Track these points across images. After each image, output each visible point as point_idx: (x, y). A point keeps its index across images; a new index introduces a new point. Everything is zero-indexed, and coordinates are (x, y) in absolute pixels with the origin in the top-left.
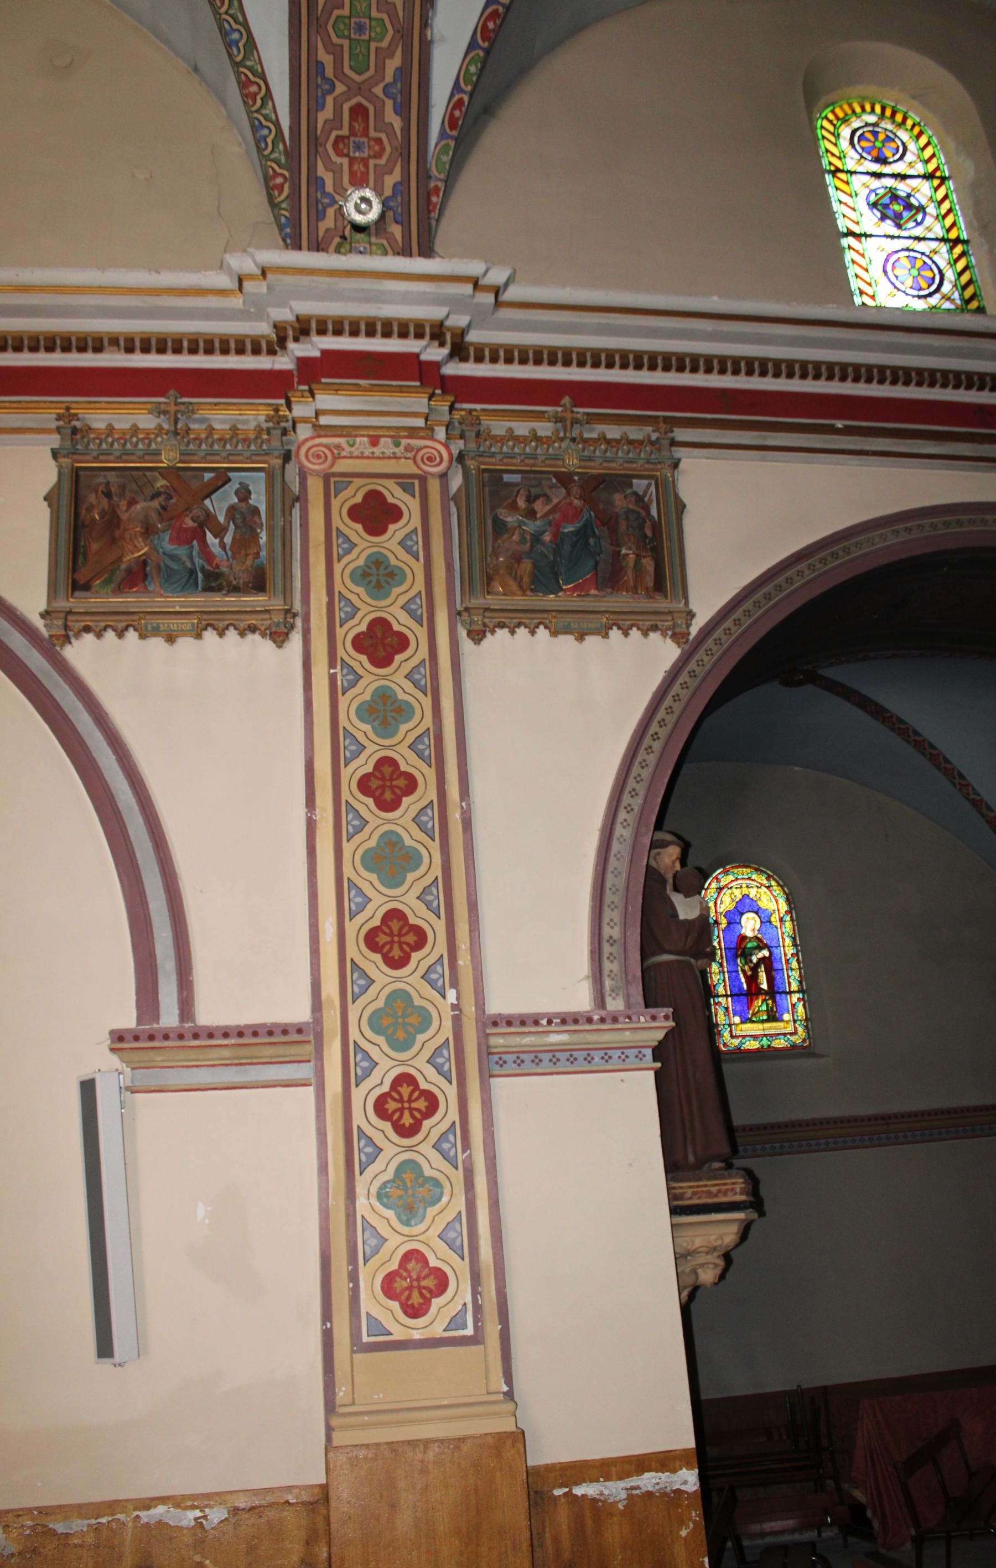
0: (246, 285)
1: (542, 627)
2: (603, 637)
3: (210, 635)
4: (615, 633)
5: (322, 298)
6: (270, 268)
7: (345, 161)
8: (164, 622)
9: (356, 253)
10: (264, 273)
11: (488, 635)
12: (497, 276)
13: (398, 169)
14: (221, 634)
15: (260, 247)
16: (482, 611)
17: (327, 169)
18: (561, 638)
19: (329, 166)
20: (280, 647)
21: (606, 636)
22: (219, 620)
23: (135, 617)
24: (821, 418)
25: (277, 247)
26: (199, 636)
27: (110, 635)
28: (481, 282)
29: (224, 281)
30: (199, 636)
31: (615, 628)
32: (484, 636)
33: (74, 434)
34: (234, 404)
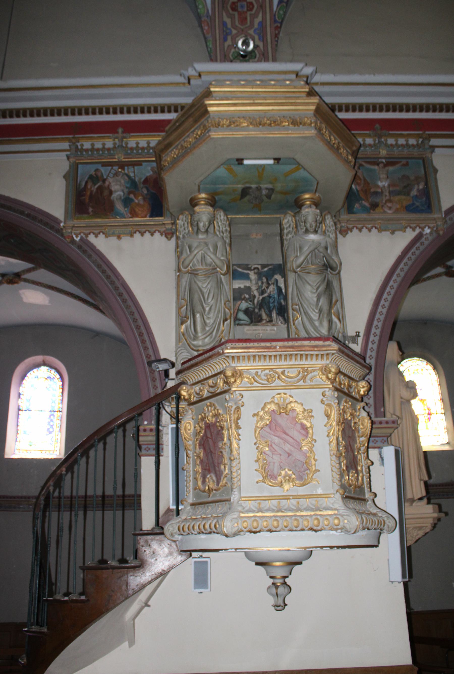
0: (192, 82)
1: (374, 228)
2: (403, 232)
3: (137, 235)
4: (137, 235)
5: (271, 88)
6: (203, 72)
7: (236, 13)
8: (117, 230)
9: (228, 61)
10: (200, 75)
11: (349, 232)
12: (308, 70)
13: (260, 15)
14: (142, 235)
15: (200, 61)
16: (346, 221)
17: (228, 17)
18: (384, 233)
19: (229, 16)
20: (344, 237)
21: (405, 231)
22: (96, 230)
23: (104, 228)
24: (410, 130)
25: (208, 62)
26: (132, 236)
27: (147, 235)
28: (299, 74)
29: (182, 80)
30: (132, 236)
31: (408, 228)
32: (347, 233)
33: (75, 152)
34: (141, 136)
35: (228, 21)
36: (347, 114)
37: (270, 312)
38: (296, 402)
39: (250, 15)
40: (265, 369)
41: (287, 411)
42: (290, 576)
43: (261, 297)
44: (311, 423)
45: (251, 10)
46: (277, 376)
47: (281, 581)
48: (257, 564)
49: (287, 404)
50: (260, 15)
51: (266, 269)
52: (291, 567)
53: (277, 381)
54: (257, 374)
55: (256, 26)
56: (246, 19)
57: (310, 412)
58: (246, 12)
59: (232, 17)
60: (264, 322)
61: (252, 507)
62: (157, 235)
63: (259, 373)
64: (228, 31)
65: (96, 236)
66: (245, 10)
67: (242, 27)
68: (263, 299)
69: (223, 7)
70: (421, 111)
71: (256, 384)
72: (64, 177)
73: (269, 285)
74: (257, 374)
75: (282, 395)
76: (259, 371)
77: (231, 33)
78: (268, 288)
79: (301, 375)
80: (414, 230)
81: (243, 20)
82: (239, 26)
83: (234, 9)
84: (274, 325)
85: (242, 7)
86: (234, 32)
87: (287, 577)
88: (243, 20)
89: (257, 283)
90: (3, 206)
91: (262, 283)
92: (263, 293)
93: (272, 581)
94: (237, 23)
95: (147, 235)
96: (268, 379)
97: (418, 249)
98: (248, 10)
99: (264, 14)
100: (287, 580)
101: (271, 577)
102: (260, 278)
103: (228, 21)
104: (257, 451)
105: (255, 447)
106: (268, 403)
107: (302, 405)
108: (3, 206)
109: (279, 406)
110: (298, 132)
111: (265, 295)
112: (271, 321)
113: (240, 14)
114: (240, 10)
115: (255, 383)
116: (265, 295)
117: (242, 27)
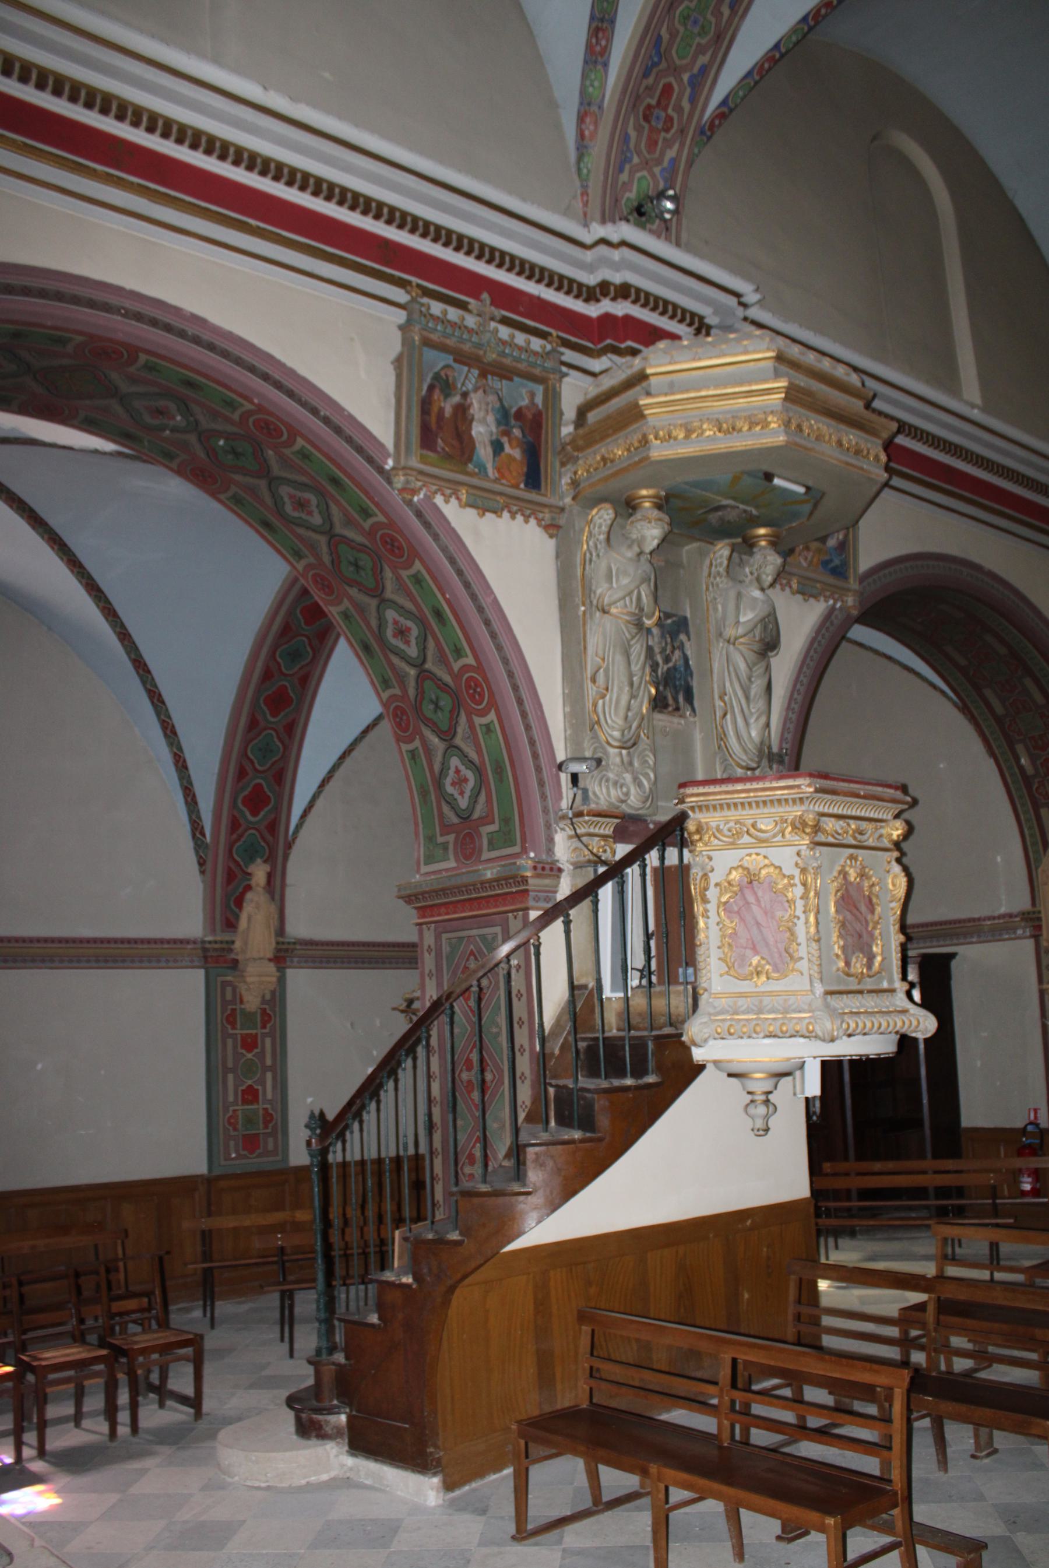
7: (646, 125)
13: (676, 147)
27: (519, 518)
35: (632, 133)
36: (205, 158)
37: (677, 693)
39: (665, 139)
42: (775, 1092)
43: (665, 668)
45: (667, 130)
47: (763, 1097)
48: (730, 1075)
50: (676, 147)
51: (669, 621)
52: (774, 1080)
55: (666, 164)
56: (656, 143)
58: (659, 132)
59: (639, 129)
60: (670, 709)
61: (751, 1006)
62: (533, 521)
64: (629, 155)
65: (447, 502)
66: (660, 126)
67: (648, 156)
68: (669, 669)
69: (634, 105)
70: (263, 173)
71: (716, 842)
72: (392, 363)
73: (674, 649)
75: (754, 856)
77: (630, 160)
78: (673, 652)
80: (826, 601)
81: (652, 144)
82: (645, 152)
83: (646, 118)
84: (681, 716)
85: (658, 118)
86: (636, 160)
87: (770, 1092)
88: (652, 144)
89: (660, 643)
90: (9, 289)
91: (666, 644)
92: (667, 660)
93: (749, 1097)
94: (643, 145)
95: (519, 518)
99: (682, 145)
100: (770, 1097)
101: (749, 1093)
102: (663, 636)
103: (632, 133)
108: (9, 289)
110: (949, 487)
111: (671, 665)
112: (677, 709)
113: (652, 129)
114: (653, 123)
116: (671, 665)
117: (648, 156)
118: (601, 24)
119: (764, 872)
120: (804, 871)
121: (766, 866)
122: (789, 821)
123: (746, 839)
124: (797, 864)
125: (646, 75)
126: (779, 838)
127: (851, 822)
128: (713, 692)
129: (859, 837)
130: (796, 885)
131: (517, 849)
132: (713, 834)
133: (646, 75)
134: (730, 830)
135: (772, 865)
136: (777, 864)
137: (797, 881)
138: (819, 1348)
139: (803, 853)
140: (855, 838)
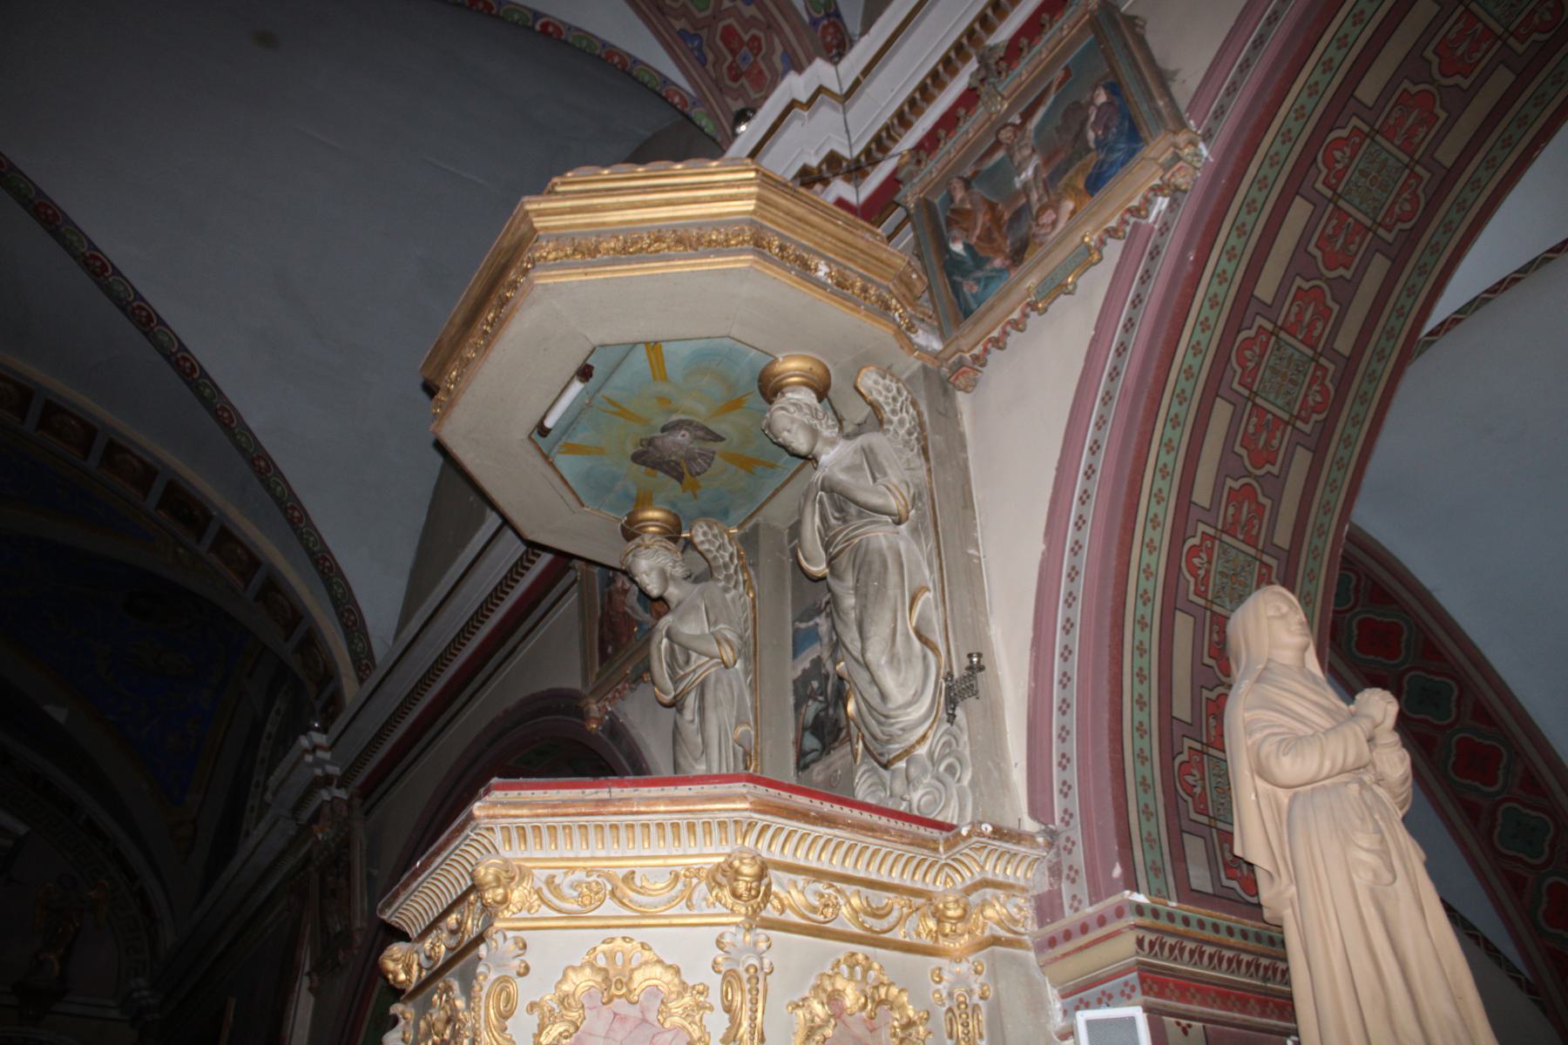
13: (777, 41)
38: (659, 962)
40: (573, 869)
41: (630, 991)
44: (702, 1027)
45: (760, 49)
46: (609, 887)
49: (633, 970)
50: (777, 41)
53: (609, 902)
54: (550, 881)
57: (701, 993)
63: (557, 881)
71: (545, 911)
74: (550, 881)
75: (619, 942)
76: (559, 874)
79: (679, 886)
96: (581, 895)
97: (1321, 531)
98: (756, 55)
99: (780, 32)
104: (529, 958)
105: (529, 958)
106: (574, 968)
107: (677, 972)
109: (606, 979)
115: (544, 908)
118: (473, 1042)
119: (638, 976)
120: (730, 978)
121: (646, 963)
122: (703, 874)
123: (610, 907)
124: (715, 964)
125: (703, 61)
126: (681, 908)
127: (849, 889)
128: (553, 586)
129: (870, 922)
130: (711, 1008)
131: (973, 240)
132: (538, 892)
133: (703, 61)
134: (574, 886)
135: (659, 962)
136: (668, 962)
137: (715, 998)
138: (557, 193)
139: (727, 939)
140: (862, 925)
